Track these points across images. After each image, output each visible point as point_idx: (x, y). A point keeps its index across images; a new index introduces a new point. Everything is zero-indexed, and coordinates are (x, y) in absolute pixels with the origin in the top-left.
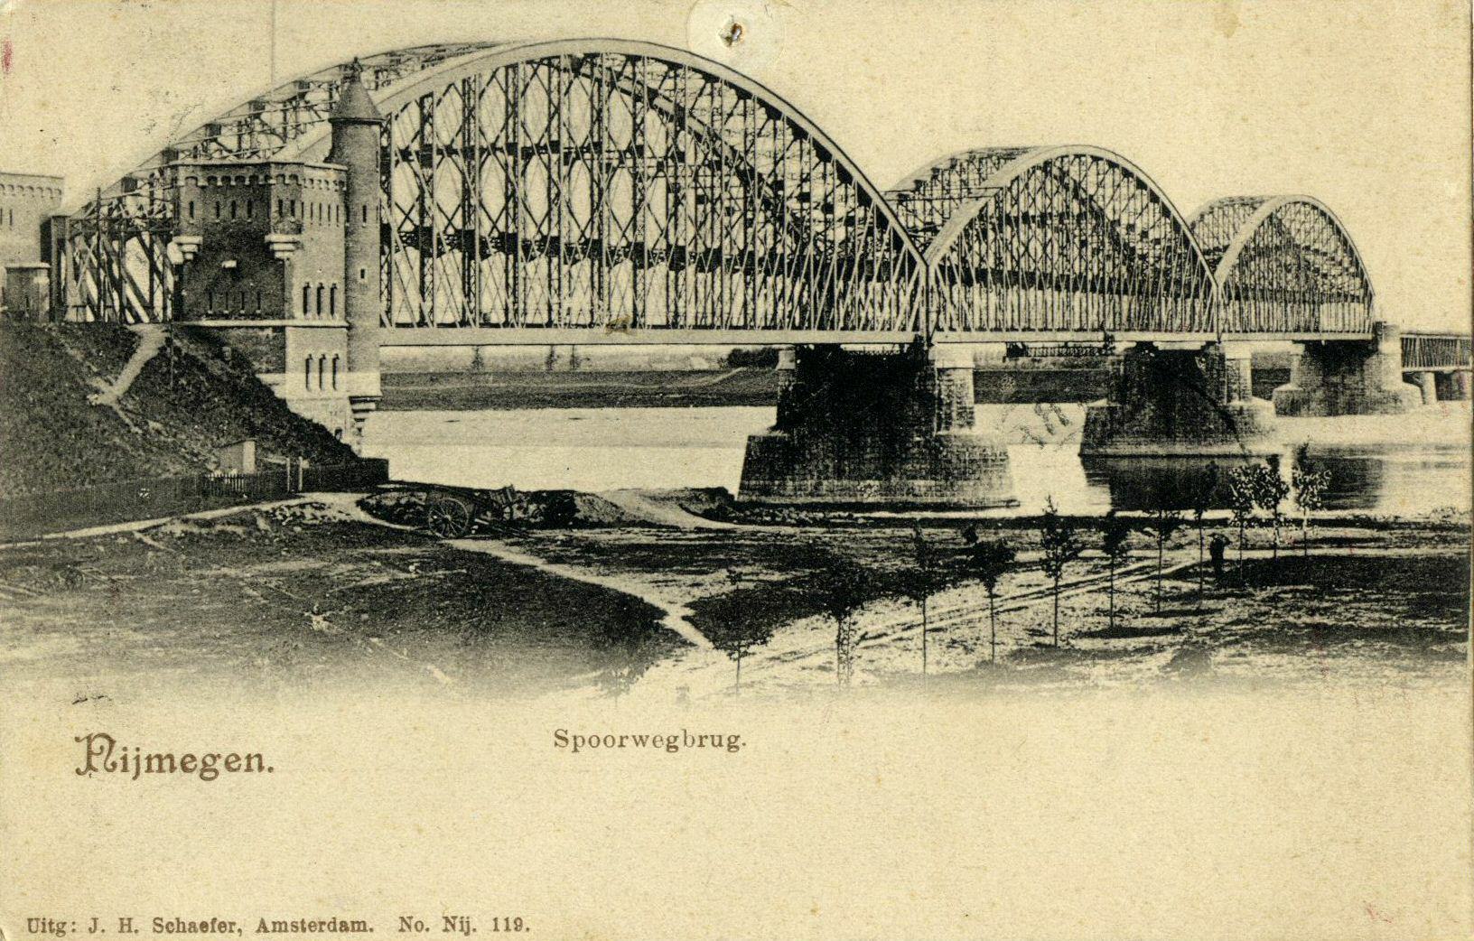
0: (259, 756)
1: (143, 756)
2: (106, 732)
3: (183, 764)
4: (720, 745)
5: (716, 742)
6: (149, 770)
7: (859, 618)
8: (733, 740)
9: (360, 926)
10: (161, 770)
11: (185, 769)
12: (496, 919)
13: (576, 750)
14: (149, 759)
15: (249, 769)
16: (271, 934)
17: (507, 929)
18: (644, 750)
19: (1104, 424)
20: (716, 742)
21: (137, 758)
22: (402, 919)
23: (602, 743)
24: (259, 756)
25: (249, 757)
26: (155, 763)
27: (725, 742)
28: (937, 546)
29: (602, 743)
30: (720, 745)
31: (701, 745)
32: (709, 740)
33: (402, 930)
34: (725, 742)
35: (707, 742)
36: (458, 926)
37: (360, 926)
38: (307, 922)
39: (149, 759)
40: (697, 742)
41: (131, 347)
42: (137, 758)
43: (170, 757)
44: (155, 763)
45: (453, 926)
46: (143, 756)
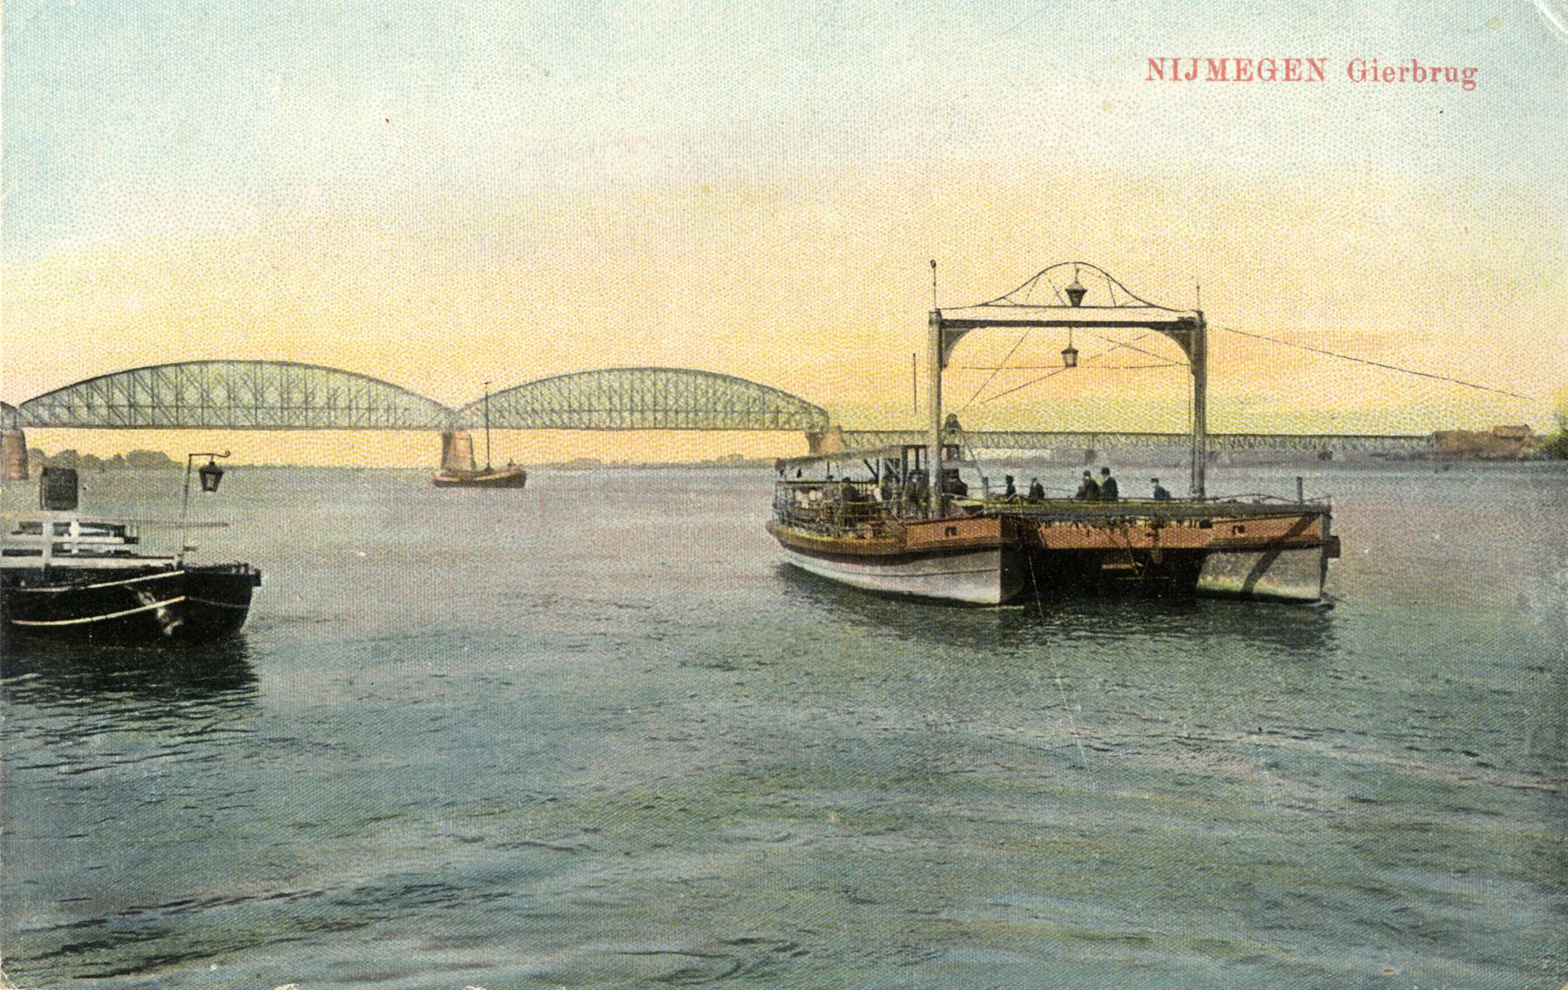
0: (1448, 79)
2: (1346, 72)
3: (1385, 74)
4: (1455, 79)
5: (1452, 77)
12: (1195, 61)
16: (1303, 56)
17: (1376, 79)
20: (1452, 77)
22: (1152, 62)
27: (1460, 76)
30: (1455, 79)
31: (1434, 79)
33: (1150, 79)
34: (1460, 76)
35: (1441, 76)
36: (1169, 73)
38: (1381, 67)
40: (1398, 76)
45: (1160, 73)
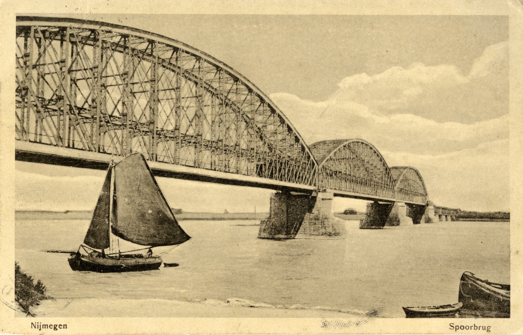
1: (42, 325)
3: (461, 327)
6: (43, 328)
7: (134, 239)
8: (55, 326)
9: (176, 265)
10: (45, 328)
11: (464, 327)
13: (40, 330)
14: (43, 325)
15: (64, 328)
18: (159, 41)
19: (99, 243)
21: (40, 325)
23: (465, 328)
24: (483, 330)
25: (64, 325)
26: (44, 326)
28: (129, 258)
29: (465, 328)
32: (482, 327)
34: (486, 329)
35: (481, 328)
37: (176, 265)
39: (43, 325)
41: (17, 295)
42: (40, 325)
43: (47, 325)
44: (44, 326)
46: (42, 325)
